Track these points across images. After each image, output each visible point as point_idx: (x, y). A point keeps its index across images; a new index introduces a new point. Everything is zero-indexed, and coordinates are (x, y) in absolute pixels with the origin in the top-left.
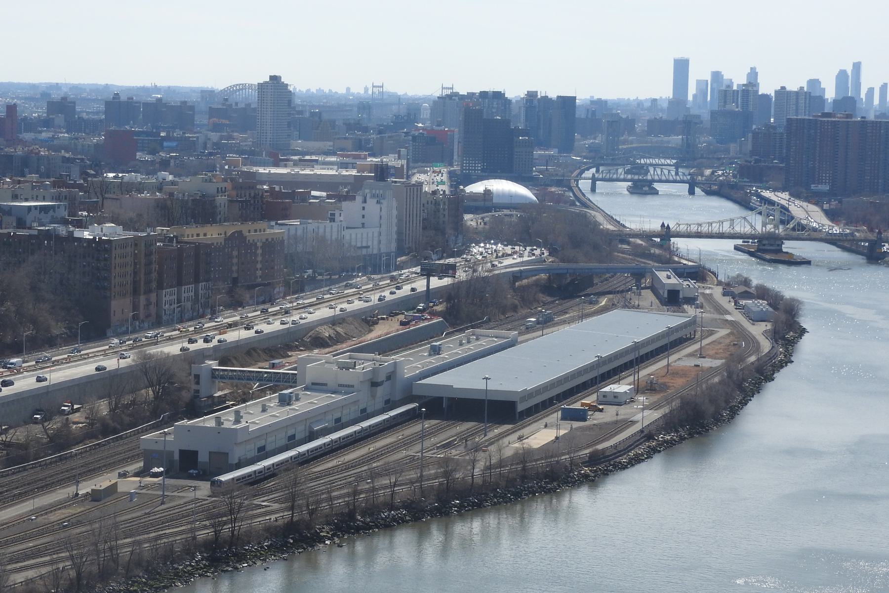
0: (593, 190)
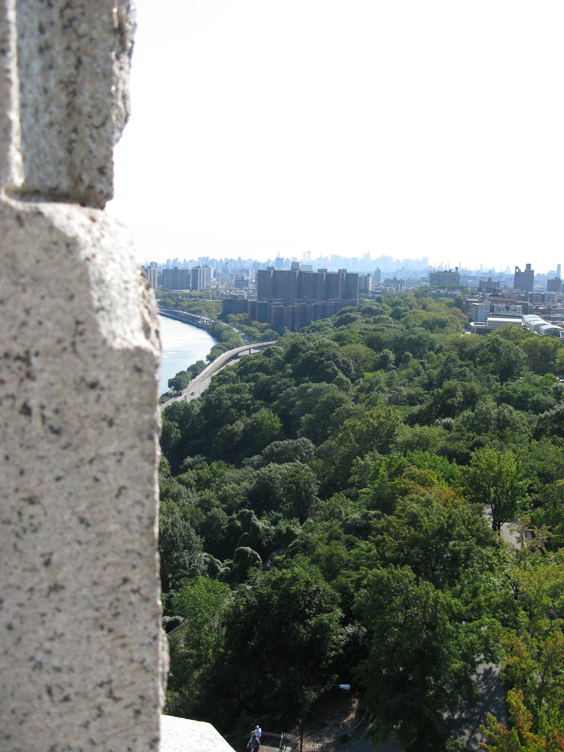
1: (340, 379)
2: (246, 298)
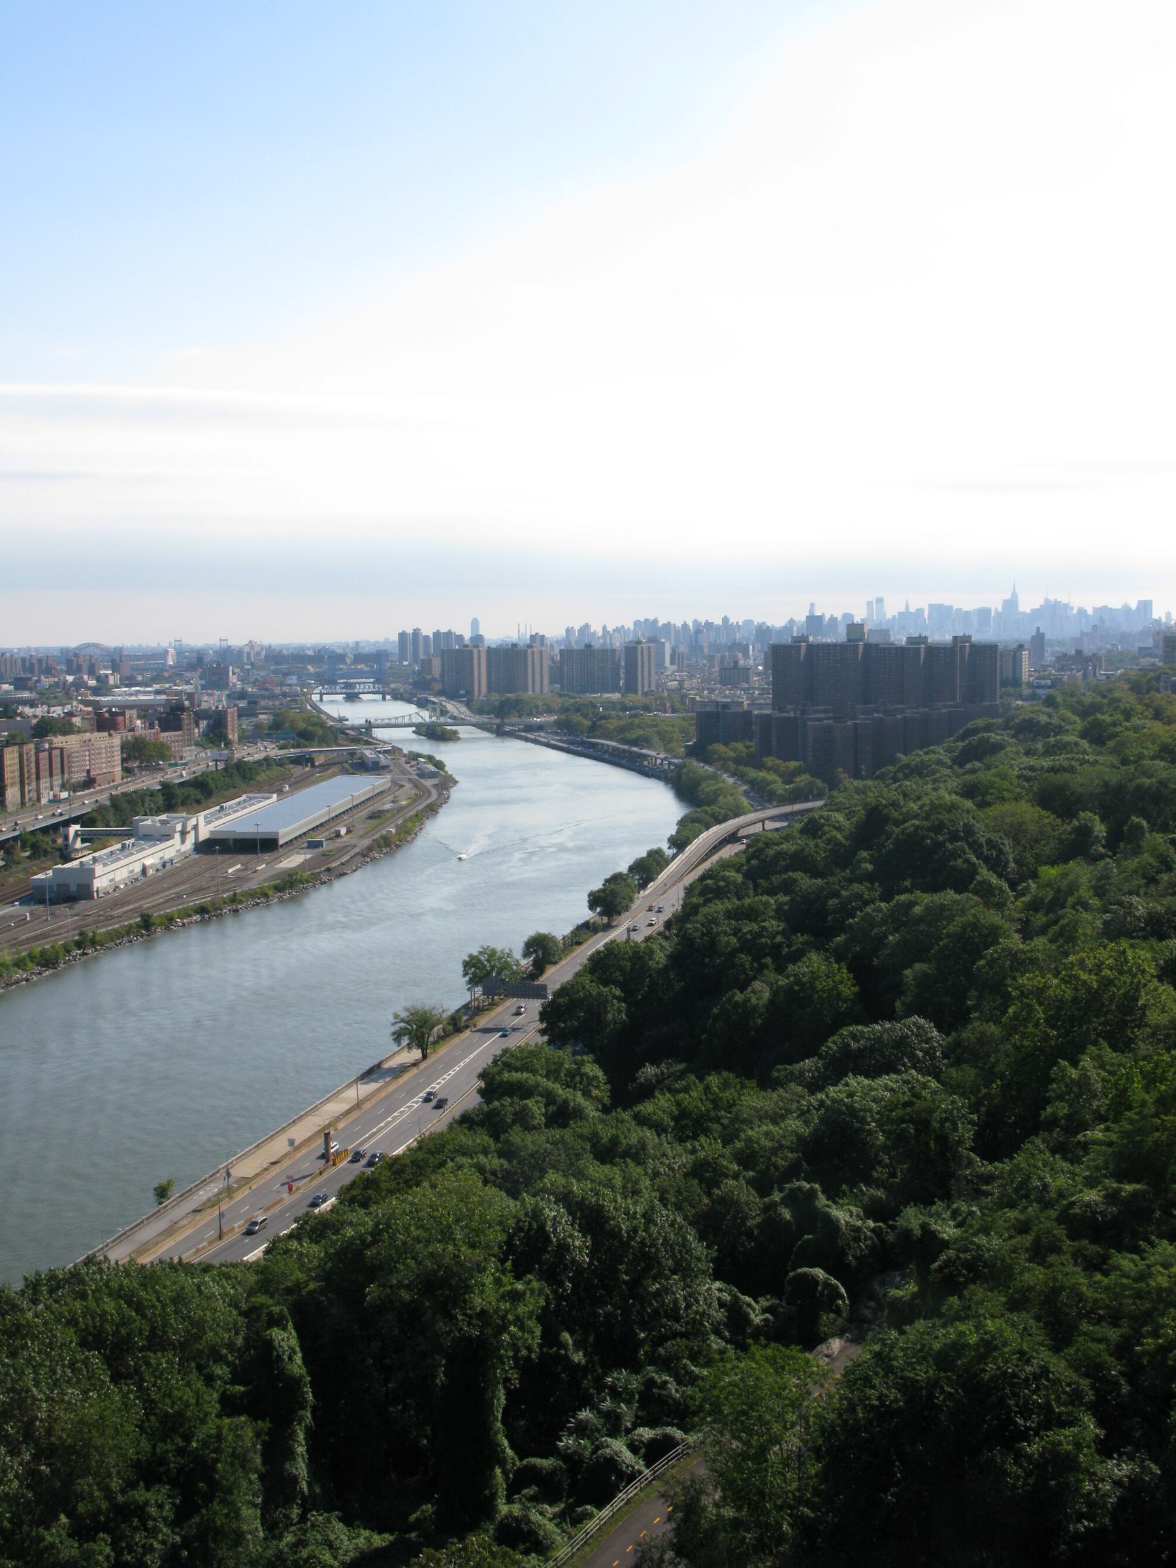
0: (321, 700)
1: (984, 882)
2: (746, 707)
